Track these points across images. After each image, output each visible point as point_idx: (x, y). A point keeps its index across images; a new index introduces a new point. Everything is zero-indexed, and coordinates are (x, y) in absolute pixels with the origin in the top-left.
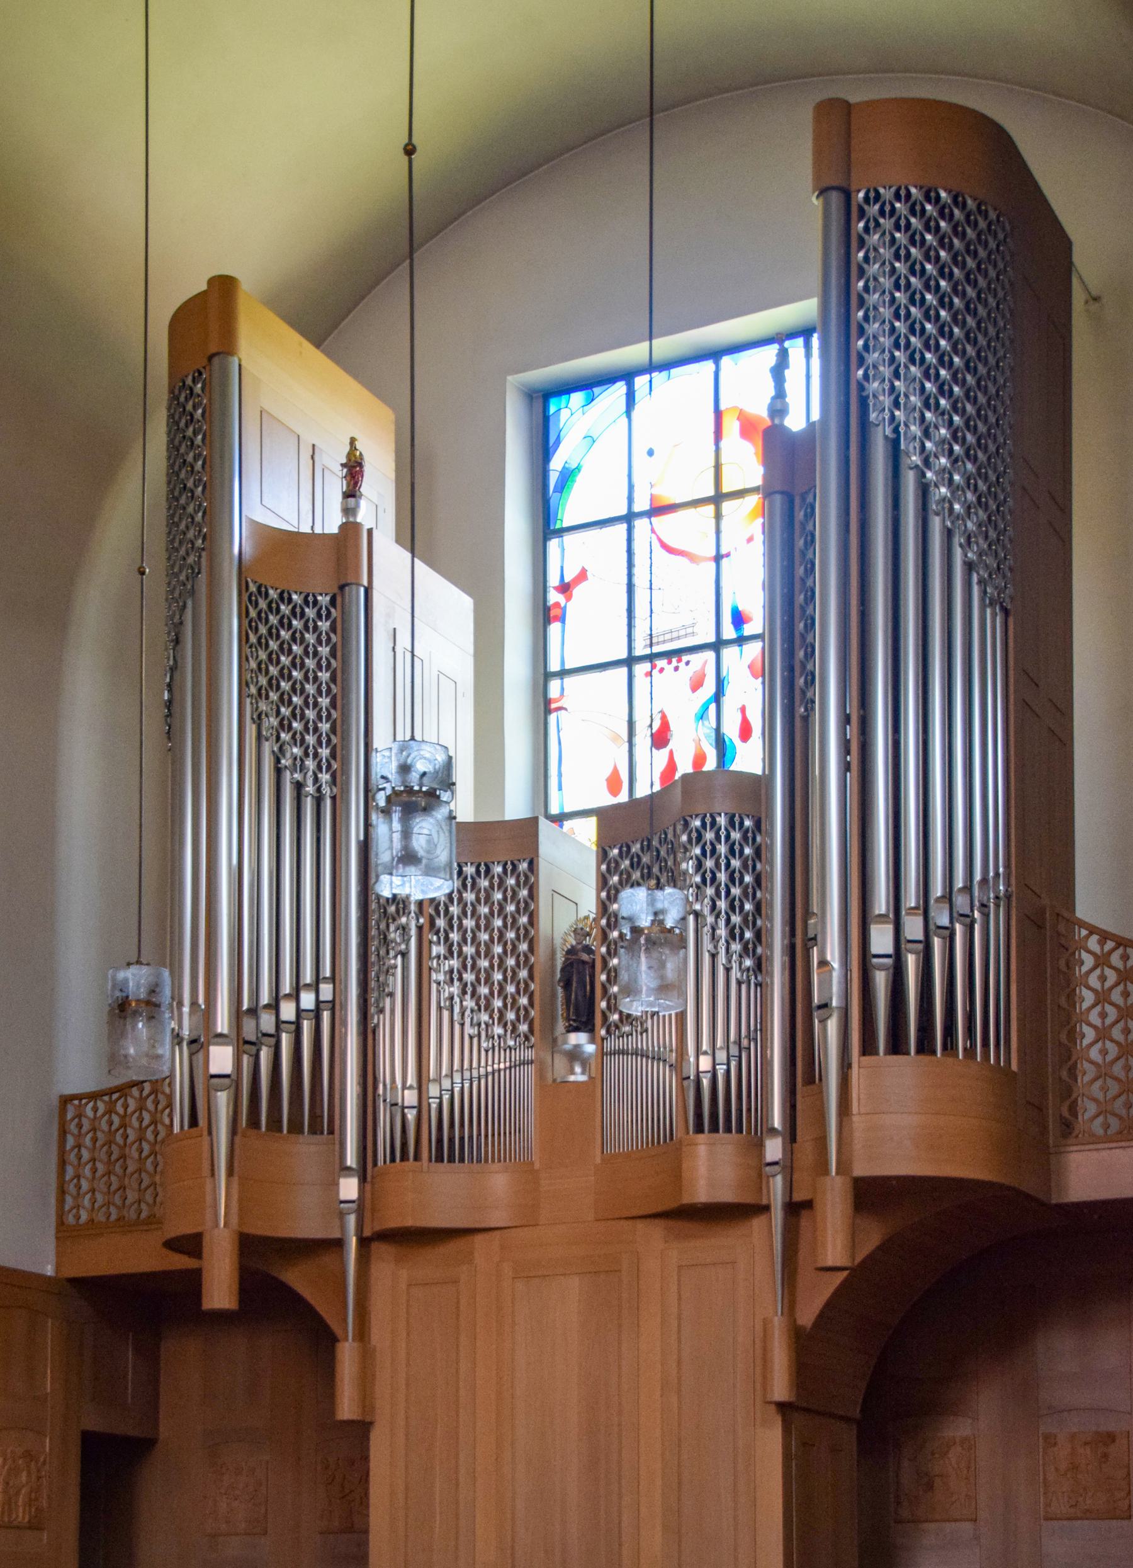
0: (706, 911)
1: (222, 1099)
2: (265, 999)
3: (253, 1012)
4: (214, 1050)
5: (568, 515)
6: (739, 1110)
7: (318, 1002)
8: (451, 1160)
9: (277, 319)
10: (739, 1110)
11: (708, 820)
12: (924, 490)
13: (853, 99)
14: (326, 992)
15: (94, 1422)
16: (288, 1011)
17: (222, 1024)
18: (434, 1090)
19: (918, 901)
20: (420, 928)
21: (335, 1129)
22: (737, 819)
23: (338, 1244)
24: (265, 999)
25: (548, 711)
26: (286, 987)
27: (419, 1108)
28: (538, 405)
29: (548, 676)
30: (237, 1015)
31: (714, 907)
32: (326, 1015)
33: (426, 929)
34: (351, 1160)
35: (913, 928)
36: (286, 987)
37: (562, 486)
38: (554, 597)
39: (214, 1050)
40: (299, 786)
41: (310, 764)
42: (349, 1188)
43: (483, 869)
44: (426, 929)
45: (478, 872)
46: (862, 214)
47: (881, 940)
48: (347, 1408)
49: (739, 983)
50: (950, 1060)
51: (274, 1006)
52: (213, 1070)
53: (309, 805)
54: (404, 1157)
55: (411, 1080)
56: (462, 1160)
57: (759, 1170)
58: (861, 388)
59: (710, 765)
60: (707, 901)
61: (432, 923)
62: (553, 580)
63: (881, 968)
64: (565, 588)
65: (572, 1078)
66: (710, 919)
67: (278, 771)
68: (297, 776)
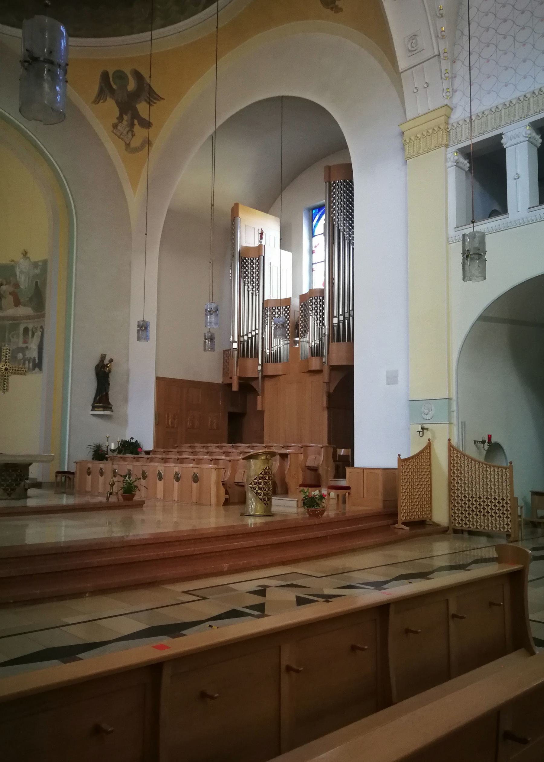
0: (313, 315)
1: (236, 352)
2: (245, 333)
3: (243, 336)
4: (234, 344)
5: (315, 234)
6: (319, 352)
7: (255, 333)
8: (278, 362)
9: (251, 209)
10: (319, 352)
11: (277, 308)
12: (344, 235)
13: (330, 165)
14: (257, 331)
15: (231, 410)
16: (250, 336)
17: (236, 339)
18: (272, 349)
19: (348, 311)
20: (270, 319)
21: (256, 356)
22: (319, 297)
23: (257, 378)
24: (245, 333)
25: (313, 271)
26: (250, 331)
27: (270, 353)
28: (311, 211)
29: (313, 264)
30: (239, 336)
31: (314, 314)
32: (257, 336)
33: (271, 319)
34: (260, 363)
35: (341, 318)
36: (250, 331)
37: (315, 227)
38: (314, 249)
39: (234, 344)
40: (252, 294)
41: (254, 289)
42: (260, 368)
43: (277, 308)
44: (271, 319)
45: (276, 309)
46: (332, 186)
47: (335, 321)
48: (259, 408)
49: (319, 328)
50: (349, 343)
51: (247, 335)
52: (234, 348)
53: (254, 297)
54: (267, 362)
55: (269, 348)
56: (278, 362)
57: (322, 363)
58: (332, 218)
59: (486, 234)
60: (313, 313)
61: (272, 319)
62: (313, 246)
63: (335, 326)
64: (316, 247)
65: (296, 346)
66: (314, 317)
67: (248, 291)
68: (252, 292)
